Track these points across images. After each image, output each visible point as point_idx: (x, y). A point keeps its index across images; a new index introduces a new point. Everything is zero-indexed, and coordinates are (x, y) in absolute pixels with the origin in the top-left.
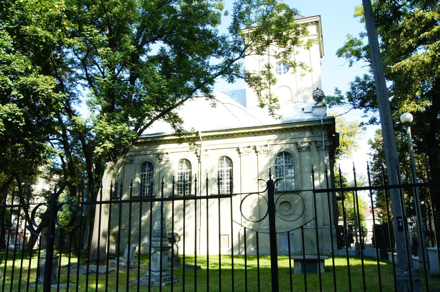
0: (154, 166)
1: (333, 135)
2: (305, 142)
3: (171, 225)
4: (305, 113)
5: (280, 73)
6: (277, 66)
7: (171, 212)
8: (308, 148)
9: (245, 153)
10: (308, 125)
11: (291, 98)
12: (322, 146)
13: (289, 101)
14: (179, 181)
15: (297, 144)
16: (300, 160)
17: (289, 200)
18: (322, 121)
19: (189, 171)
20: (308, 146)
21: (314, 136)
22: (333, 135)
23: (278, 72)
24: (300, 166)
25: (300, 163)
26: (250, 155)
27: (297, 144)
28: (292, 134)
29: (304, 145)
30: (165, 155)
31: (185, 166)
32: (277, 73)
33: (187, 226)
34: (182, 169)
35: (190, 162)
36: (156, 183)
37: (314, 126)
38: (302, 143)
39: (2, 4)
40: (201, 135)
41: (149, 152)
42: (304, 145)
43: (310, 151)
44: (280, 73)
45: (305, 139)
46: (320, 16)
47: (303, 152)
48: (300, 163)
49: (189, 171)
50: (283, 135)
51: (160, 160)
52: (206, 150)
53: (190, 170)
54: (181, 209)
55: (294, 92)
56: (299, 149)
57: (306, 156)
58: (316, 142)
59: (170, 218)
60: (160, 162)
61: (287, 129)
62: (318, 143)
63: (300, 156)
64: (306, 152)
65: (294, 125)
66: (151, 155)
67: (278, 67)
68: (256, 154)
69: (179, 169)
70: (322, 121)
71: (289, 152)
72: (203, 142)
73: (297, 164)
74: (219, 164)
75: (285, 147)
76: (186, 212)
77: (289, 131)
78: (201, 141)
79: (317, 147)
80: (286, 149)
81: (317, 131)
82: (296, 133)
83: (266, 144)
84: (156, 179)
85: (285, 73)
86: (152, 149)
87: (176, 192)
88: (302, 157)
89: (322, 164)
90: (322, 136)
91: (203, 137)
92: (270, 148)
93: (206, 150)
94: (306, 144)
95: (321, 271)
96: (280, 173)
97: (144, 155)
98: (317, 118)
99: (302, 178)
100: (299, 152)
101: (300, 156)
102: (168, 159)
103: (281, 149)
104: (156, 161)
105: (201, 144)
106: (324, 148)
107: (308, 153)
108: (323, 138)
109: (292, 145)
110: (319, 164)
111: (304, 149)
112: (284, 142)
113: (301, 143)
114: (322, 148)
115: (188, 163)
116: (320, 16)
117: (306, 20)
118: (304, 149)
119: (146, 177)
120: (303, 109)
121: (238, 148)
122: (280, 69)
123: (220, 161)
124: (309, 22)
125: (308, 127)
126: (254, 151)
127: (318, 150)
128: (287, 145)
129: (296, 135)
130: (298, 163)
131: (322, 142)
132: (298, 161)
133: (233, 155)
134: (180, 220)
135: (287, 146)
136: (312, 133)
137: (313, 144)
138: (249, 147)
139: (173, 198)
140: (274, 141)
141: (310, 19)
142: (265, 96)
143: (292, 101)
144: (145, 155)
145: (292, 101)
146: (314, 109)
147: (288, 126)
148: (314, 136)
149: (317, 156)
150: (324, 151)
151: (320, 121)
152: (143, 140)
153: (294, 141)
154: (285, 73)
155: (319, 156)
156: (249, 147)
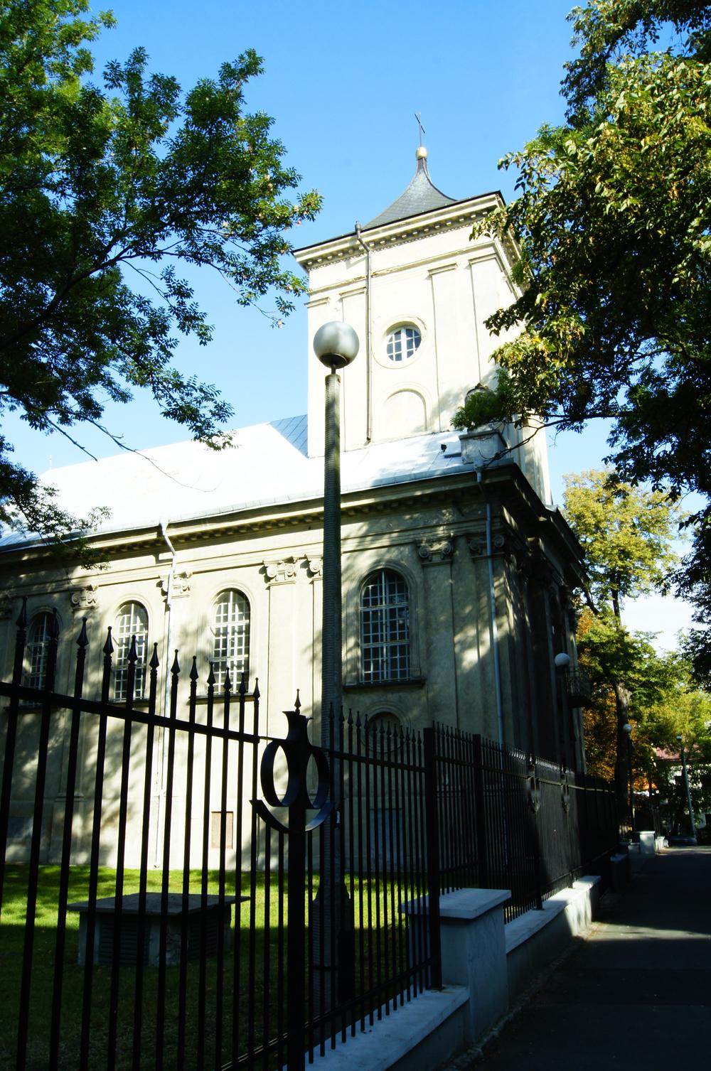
0: (60, 624)
1: (542, 519)
2: (439, 540)
3: (93, 787)
4: (446, 457)
5: (399, 357)
6: (391, 340)
7: (95, 748)
8: (448, 556)
9: (280, 578)
10: (443, 489)
11: (423, 422)
12: (484, 547)
13: (418, 430)
14: (120, 662)
15: (416, 544)
16: (427, 590)
17: (393, 710)
18: (479, 475)
19: (244, 622)
20: (446, 550)
21: (464, 519)
22: (542, 519)
23: (394, 353)
24: (426, 608)
25: (426, 598)
26: (292, 582)
27: (416, 544)
28: (407, 517)
29: (436, 547)
30: (86, 594)
31: (234, 611)
32: (391, 357)
33: (132, 788)
34: (226, 619)
35: (246, 599)
36: (62, 670)
37: (463, 490)
38: (431, 542)
39: (708, 353)
40: (168, 534)
41: (50, 588)
42: (436, 547)
43: (451, 563)
44: (399, 357)
45: (441, 531)
46: (499, 193)
47: (433, 569)
48: (426, 598)
49: (244, 622)
50: (383, 522)
51: (76, 607)
52: (184, 575)
53: (248, 621)
54: (119, 740)
55: (433, 402)
56: (425, 560)
57: (442, 580)
58: (468, 536)
59: (93, 766)
60: (74, 612)
61: (395, 502)
62: (476, 539)
63: (425, 581)
64: (441, 568)
65: (406, 491)
66: (56, 596)
67: (394, 342)
68: (311, 580)
69: (218, 619)
70: (479, 475)
71: (398, 569)
72: (177, 553)
73: (416, 603)
74: (219, 612)
75: (387, 557)
76: (132, 748)
77: (366, 513)
78: (168, 550)
79: (472, 552)
80: (389, 561)
81: (474, 506)
82: (416, 515)
83: (288, 556)
84: (63, 658)
85: (410, 354)
86: (59, 578)
87: (112, 693)
88: (431, 582)
89: (484, 600)
90: (486, 519)
91: (175, 540)
92: (350, 561)
93: (184, 575)
94: (442, 545)
95: (166, 1032)
96: (375, 630)
97: (40, 594)
98: (468, 469)
99: (429, 644)
100: (423, 567)
101: (425, 581)
102: (93, 604)
103: (378, 562)
104: (67, 611)
105: (171, 560)
106: (489, 553)
107: (446, 570)
108: (488, 523)
109: (406, 550)
110: (479, 599)
111: (436, 559)
112: (385, 541)
113: (428, 541)
114: (484, 555)
115: (140, 609)
116: (499, 193)
117: (462, 208)
118: (436, 559)
119: (229, 637)
120: (444, 447)
121: (305, 557)
122: (399, 346)
123: (222, 604)
124: (471, 213)
125: (446, 493)
126: (305, 571)
127: (474, 561)
128: (393, 549)
129: (415, 520)
130: (420, 602)
131: (484, 534)
132: (421, 594)
133: (250, 583)
134: (115, 770)
135: (394, 554)
136: (460, 510)
137: (462, 542)
138: (290, 560)
139: (103, 708)
140: (357, 540)
141: (474, 205)
142: (209, 415)
143: (426, 429)
144: (42, 594)
145: (426, 429)
146: (465, 442)
147: (393, 493)
148: (464, 519)
149: (472, 577)
150: (490, 562)
151: (473, 474)
152: (34, 556)
153: (411, 536)
154: (410, 354)
155: (477, 578)
156: (290, 560)
